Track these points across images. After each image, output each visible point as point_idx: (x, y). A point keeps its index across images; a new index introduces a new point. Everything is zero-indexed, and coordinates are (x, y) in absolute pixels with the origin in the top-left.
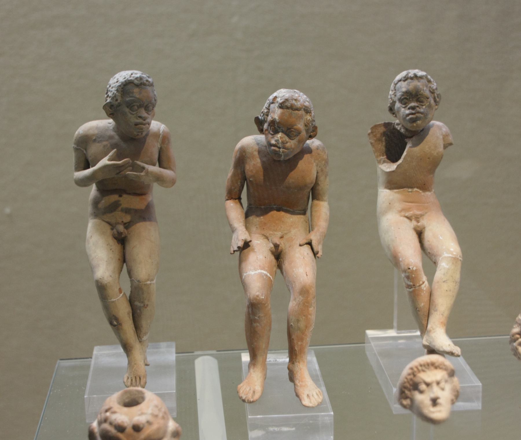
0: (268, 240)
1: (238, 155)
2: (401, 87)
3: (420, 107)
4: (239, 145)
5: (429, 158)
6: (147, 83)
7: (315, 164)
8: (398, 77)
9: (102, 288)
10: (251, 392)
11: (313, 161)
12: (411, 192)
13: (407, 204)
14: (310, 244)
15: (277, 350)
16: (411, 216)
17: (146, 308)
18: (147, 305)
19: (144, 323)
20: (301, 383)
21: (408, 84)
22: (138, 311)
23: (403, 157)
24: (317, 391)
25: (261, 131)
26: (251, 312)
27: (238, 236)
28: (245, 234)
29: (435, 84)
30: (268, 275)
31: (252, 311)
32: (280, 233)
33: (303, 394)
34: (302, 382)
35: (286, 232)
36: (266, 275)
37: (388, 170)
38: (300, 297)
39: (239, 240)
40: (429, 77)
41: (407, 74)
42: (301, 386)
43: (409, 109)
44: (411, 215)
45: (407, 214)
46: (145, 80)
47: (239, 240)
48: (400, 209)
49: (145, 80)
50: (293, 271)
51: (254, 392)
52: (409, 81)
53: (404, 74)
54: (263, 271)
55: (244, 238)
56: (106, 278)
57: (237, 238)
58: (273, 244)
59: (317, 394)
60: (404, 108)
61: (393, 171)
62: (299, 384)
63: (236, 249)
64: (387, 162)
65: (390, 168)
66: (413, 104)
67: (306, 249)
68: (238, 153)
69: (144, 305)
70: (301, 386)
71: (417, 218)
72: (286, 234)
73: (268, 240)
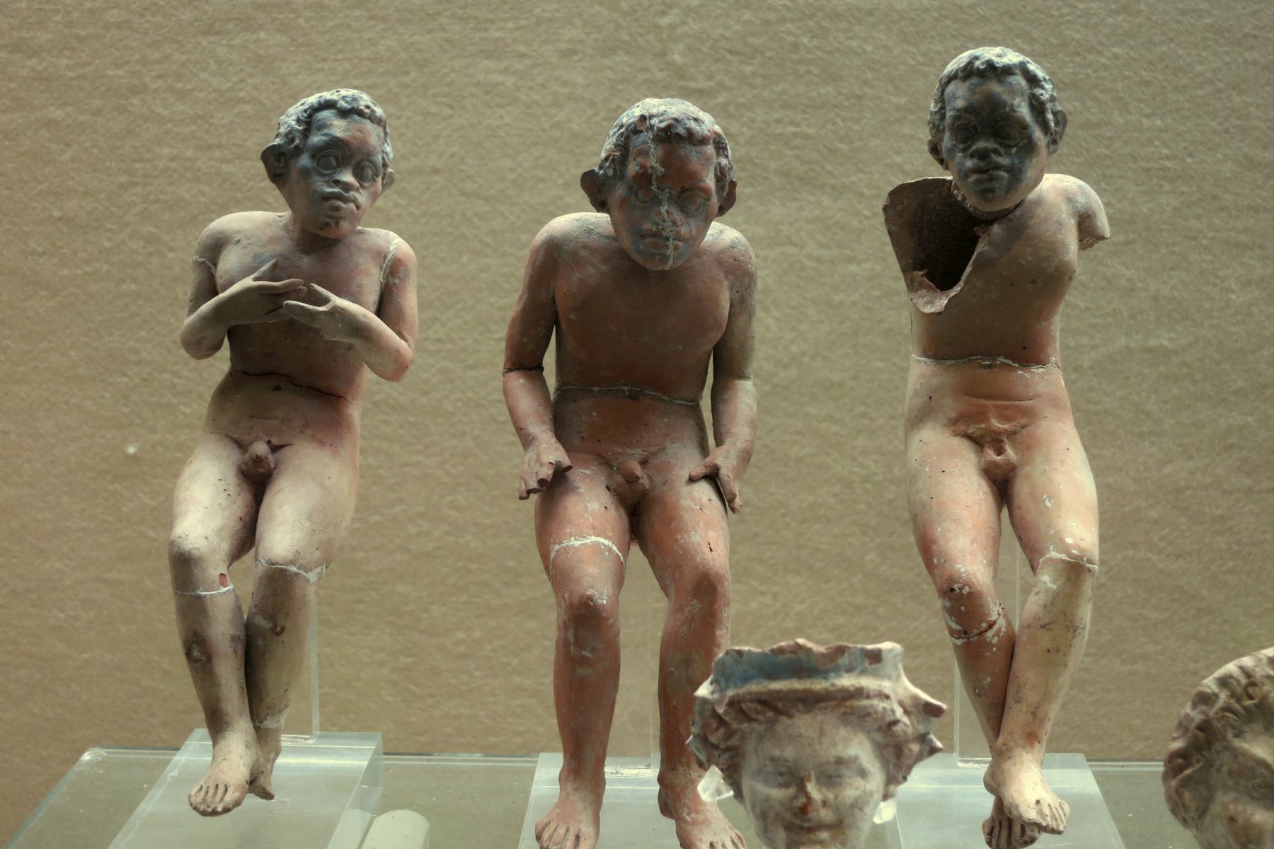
0: (611, 467)
1: (540, 258)
2: (954, 97)
3: (1002, 151)
4: (543, 234)
5: (1033, 282)
6: (367, 111)
7: (726, 283)
8: (952, 66)
9: (184, 565)
10: (571, 837)
11: (722, 277)
12: (990, 366)
13: (974, 400)
14: (712, 476)
15: (631, 754)
16: (982, 436)
17: (278, 634)
18: (283, 629)
19: (272, 676)
20: (693, 815)
21: (972, 91)
22: (260, 642)
23: (964, 278)
24: (734, 836)
25: (601, 206)
26: (571, 639)
27: (538, 456)
28: (556, 450)
29: (1048, 86)
30: (615, 548)
31: (576, 637)
32: (640, 451)
33: (701, 840)
34: (697, 812)
35: (653, 449)
36: (610, 550)
37: (929, 309)
38: (695, 602)
39: (542, 465)
40: (1032, 67)
41: (970, 63)
42: (694, 823)
43: (972, 156)
44: (979, 433)
45: (971, 431)
46: (363, 103)
47: (542, 465)
48: (953, 415)
49: (363, 103)
50: (677, 541)
51: (578, 838)
52: (975, 80)
53: (964, 57)
54: (601, 540)
55: (552, 459)
56: (192, 538)
57: (538, 459)
58: (623, 476)
59: (734, 843)
60: (964, 150)
61: (939, 314)
62: (688, 818)
63: (534, 485)
64: (929, 288)
65: (931, 303)
66: (982, 144)
67: (704, 491)
68: (541, 253)
69: (275, 626)
70: (694, 823)
71: (997, 443)
72: (654, 454)
73: (611, 467)
